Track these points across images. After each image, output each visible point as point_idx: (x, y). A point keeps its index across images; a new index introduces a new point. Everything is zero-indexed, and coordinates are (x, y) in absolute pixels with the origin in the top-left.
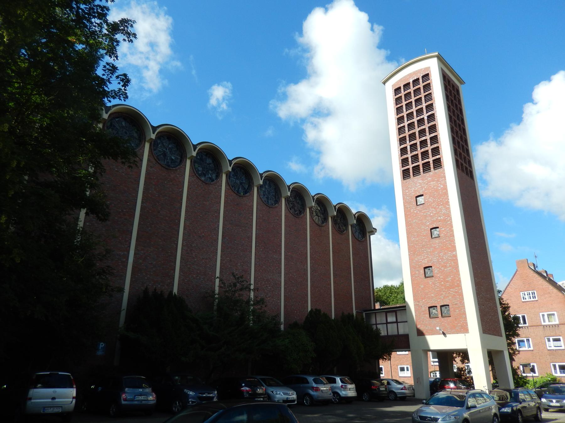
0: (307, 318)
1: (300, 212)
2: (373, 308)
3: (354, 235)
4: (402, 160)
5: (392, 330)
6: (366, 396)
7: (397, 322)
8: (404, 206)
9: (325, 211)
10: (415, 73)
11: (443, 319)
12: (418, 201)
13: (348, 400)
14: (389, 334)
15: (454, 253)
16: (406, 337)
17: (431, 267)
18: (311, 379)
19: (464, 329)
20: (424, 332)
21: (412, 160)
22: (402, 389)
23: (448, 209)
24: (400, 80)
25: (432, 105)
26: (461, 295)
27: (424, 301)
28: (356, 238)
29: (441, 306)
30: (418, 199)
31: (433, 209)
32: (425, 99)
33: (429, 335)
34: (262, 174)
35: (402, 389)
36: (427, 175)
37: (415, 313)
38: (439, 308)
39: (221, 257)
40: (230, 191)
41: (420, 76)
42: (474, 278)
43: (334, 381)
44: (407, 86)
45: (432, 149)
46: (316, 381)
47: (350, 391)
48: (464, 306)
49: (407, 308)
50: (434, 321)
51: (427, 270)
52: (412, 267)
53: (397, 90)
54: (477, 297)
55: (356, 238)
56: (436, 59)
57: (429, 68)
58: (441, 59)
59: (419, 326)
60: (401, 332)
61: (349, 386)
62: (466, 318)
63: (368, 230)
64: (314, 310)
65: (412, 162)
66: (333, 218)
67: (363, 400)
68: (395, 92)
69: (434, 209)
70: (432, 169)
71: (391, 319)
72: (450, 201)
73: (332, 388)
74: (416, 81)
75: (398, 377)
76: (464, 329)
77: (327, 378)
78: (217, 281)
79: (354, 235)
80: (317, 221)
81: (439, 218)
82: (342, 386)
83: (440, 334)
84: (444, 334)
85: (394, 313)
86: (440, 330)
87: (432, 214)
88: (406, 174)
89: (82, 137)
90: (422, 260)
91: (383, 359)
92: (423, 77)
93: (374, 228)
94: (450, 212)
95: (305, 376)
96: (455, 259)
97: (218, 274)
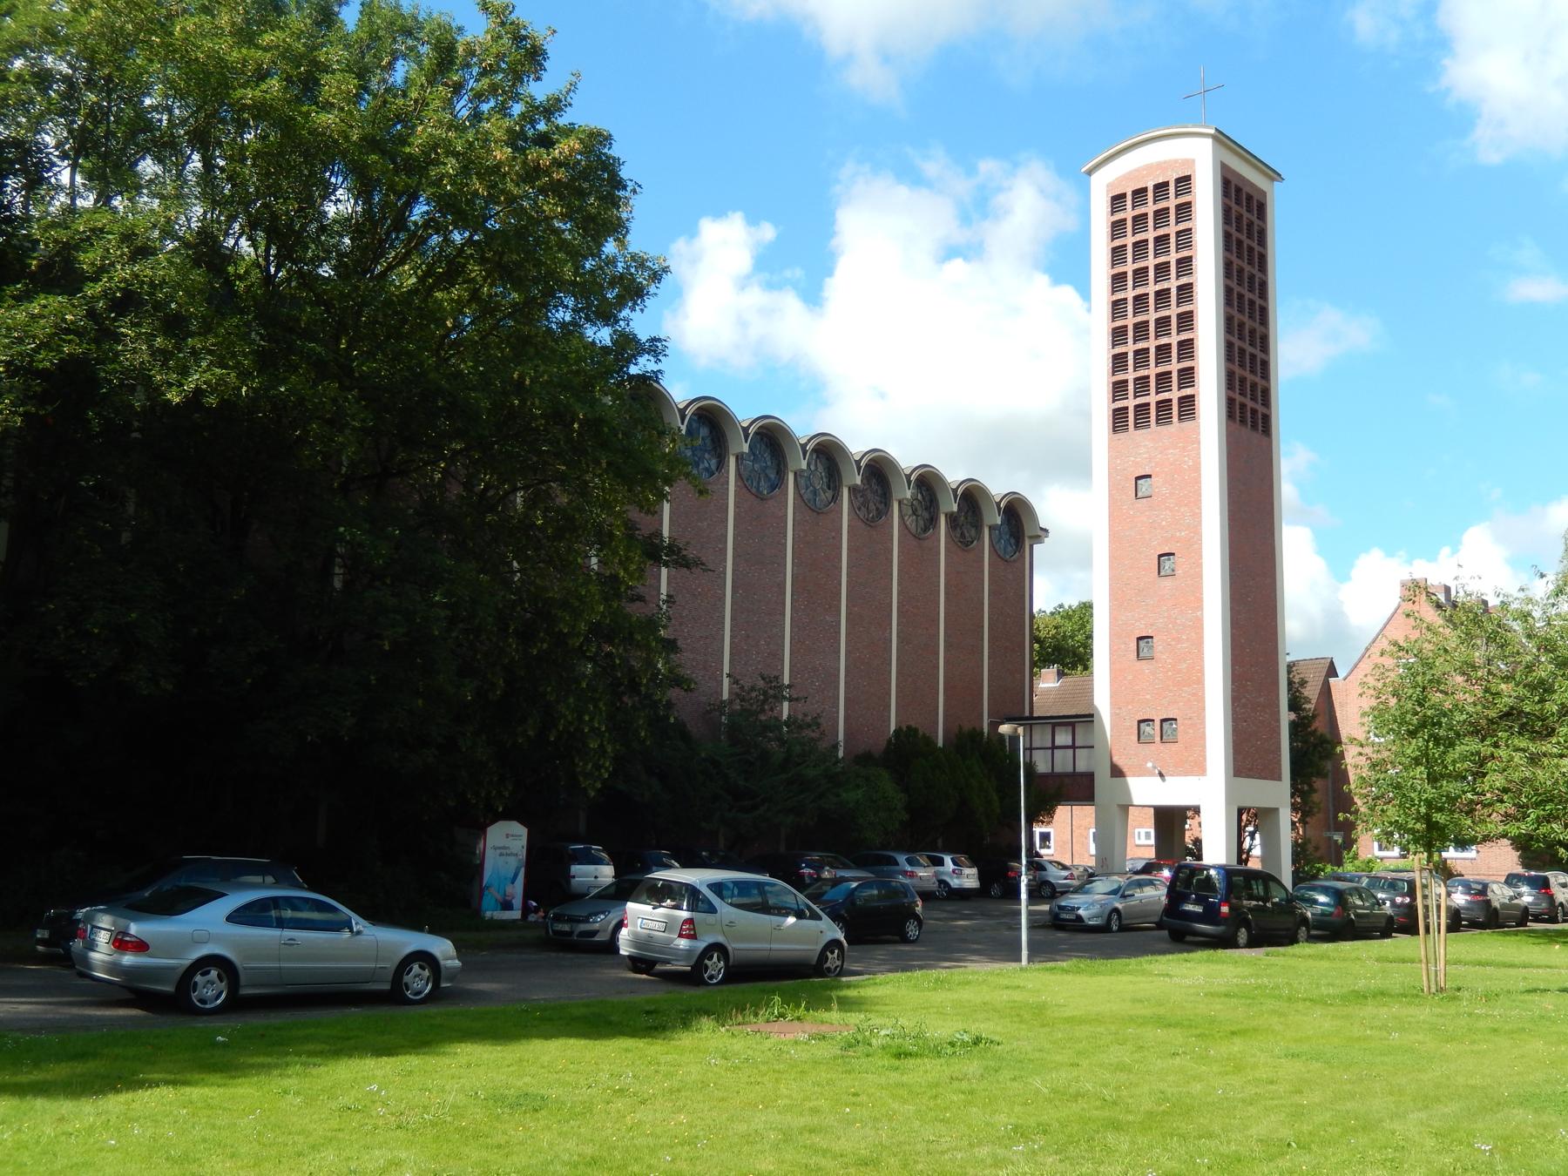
0: (889, 741)
1: (880, 514)
2: (1027, 714)
3: (994, 547)
4: (1115, 384)
5: (1063, 762)
6: (995, 890)
7: (1073, 747)
8: (1111, 495)
9: (931, 501)
10: (1161, 166)
11: (1162, 747)
12: (1139, 487)
13: (963, 894)
14: (1055, 770)
15: (1199, 613)
16: (1089, 777)
17: (1152, 637)
18: (902, 859)
19: (1199, 768)
20: (1125, 770)
21: (1135, 389)
22: (1066, 878)
23: (1197, 516)
24: (1127, 177)
25: (1189, 259)
26: (1200, 699)
27: (1130, 707)
28: (999, 556)
29: (1163, 721)
30: (1140, 482)
31: (1168, 512)
32: (1177, 241)
33: (1134, 775)
34: (806, 444)
35: (1066, 878)
36: (1164, 429)
37: (1111, 730)
38: (1157, 723)
39: (731, 631)
40: (744, 490)
41: (1171, 177)
42: (1233, 665)
43: (940, 862)
44: (1140, 193)
45: (1180, 371)
46: (910, 862)
47: (969, 878)
48: (1203, 723)
49: (1095, 719)
50: (1146, 749)
51: (1142, 643)
52: (1114, 635)
53: (1117, 201)
54: (1233, 705)
55: (999, 556)
56: (1209, 141)
57: (1193, 161)
58: (1222, 140)
59: (1115, 759)
60: (1081, 767)
61: (967, 871)
62: (1204, 747)
63: (1028, 532)
64: (905, 729)
65: (1135, 393)
66: (952, 519)
67: (992, 897)
68: (1112, 204)
69: (1171, 511)
70: (1175, 419)
71: (1063, 738)
72: (1204, 498)
73: (936, 874)
74: (1161, 188)
75: (1087, 855)
76: (1199, 768)
77: (929, 857)
78: (726, 681)
79: (994, 547)
80: (913, 528)
81: (1178, 534)
82: (954, 871)
83: (1152, 775)
84: (1161, 775)
85: (1070, 728)
86: (1155, 767)
87: (1164, 523)
88: (1119, 419)
89: (359, 320)
90: (1136, 621)
91: (1038, 821)
92: (1178, 181)
93: (1041, 529)
94: (1200, 523)
95: (892, 854)
96: (1198, 625)
97: (726, 670)
